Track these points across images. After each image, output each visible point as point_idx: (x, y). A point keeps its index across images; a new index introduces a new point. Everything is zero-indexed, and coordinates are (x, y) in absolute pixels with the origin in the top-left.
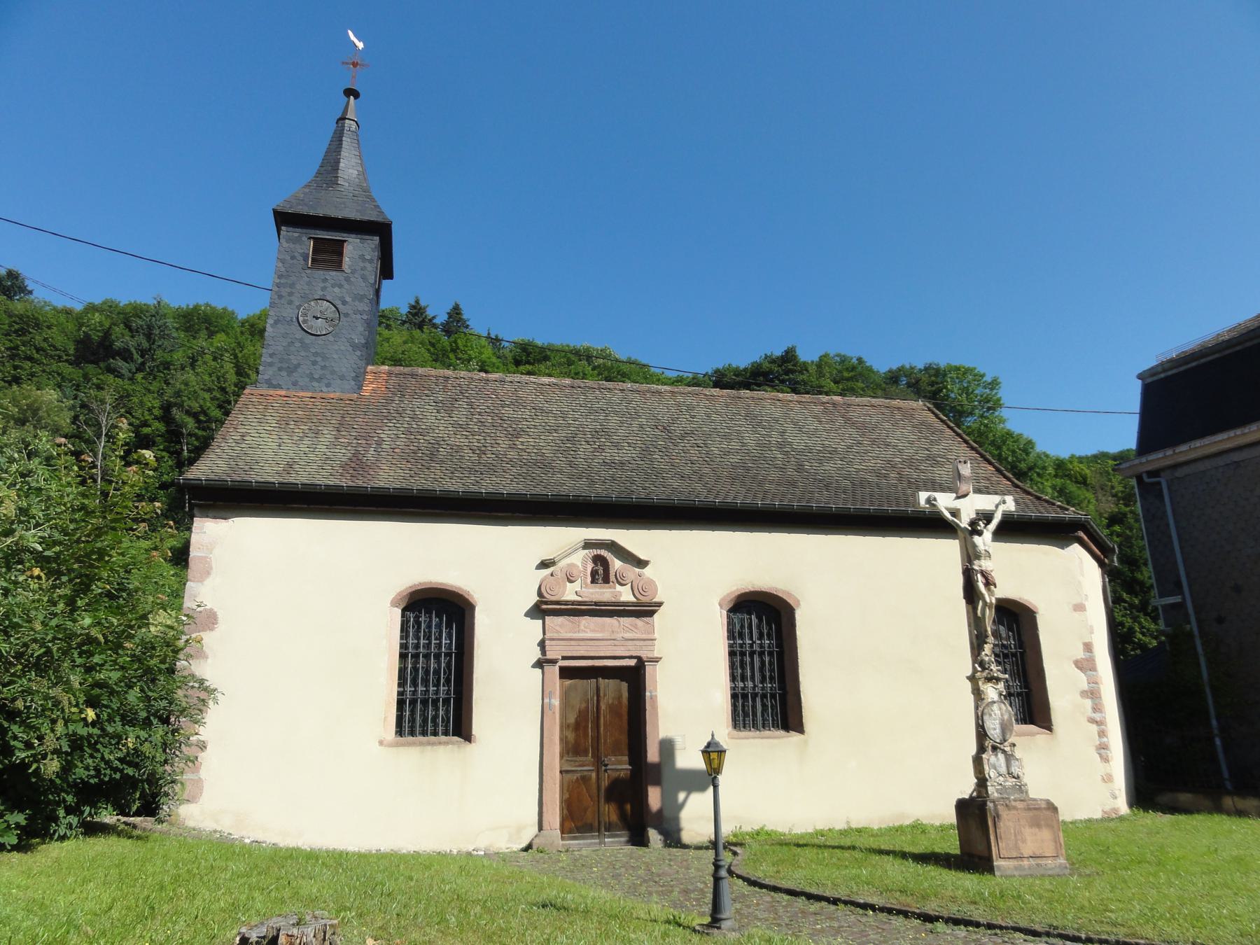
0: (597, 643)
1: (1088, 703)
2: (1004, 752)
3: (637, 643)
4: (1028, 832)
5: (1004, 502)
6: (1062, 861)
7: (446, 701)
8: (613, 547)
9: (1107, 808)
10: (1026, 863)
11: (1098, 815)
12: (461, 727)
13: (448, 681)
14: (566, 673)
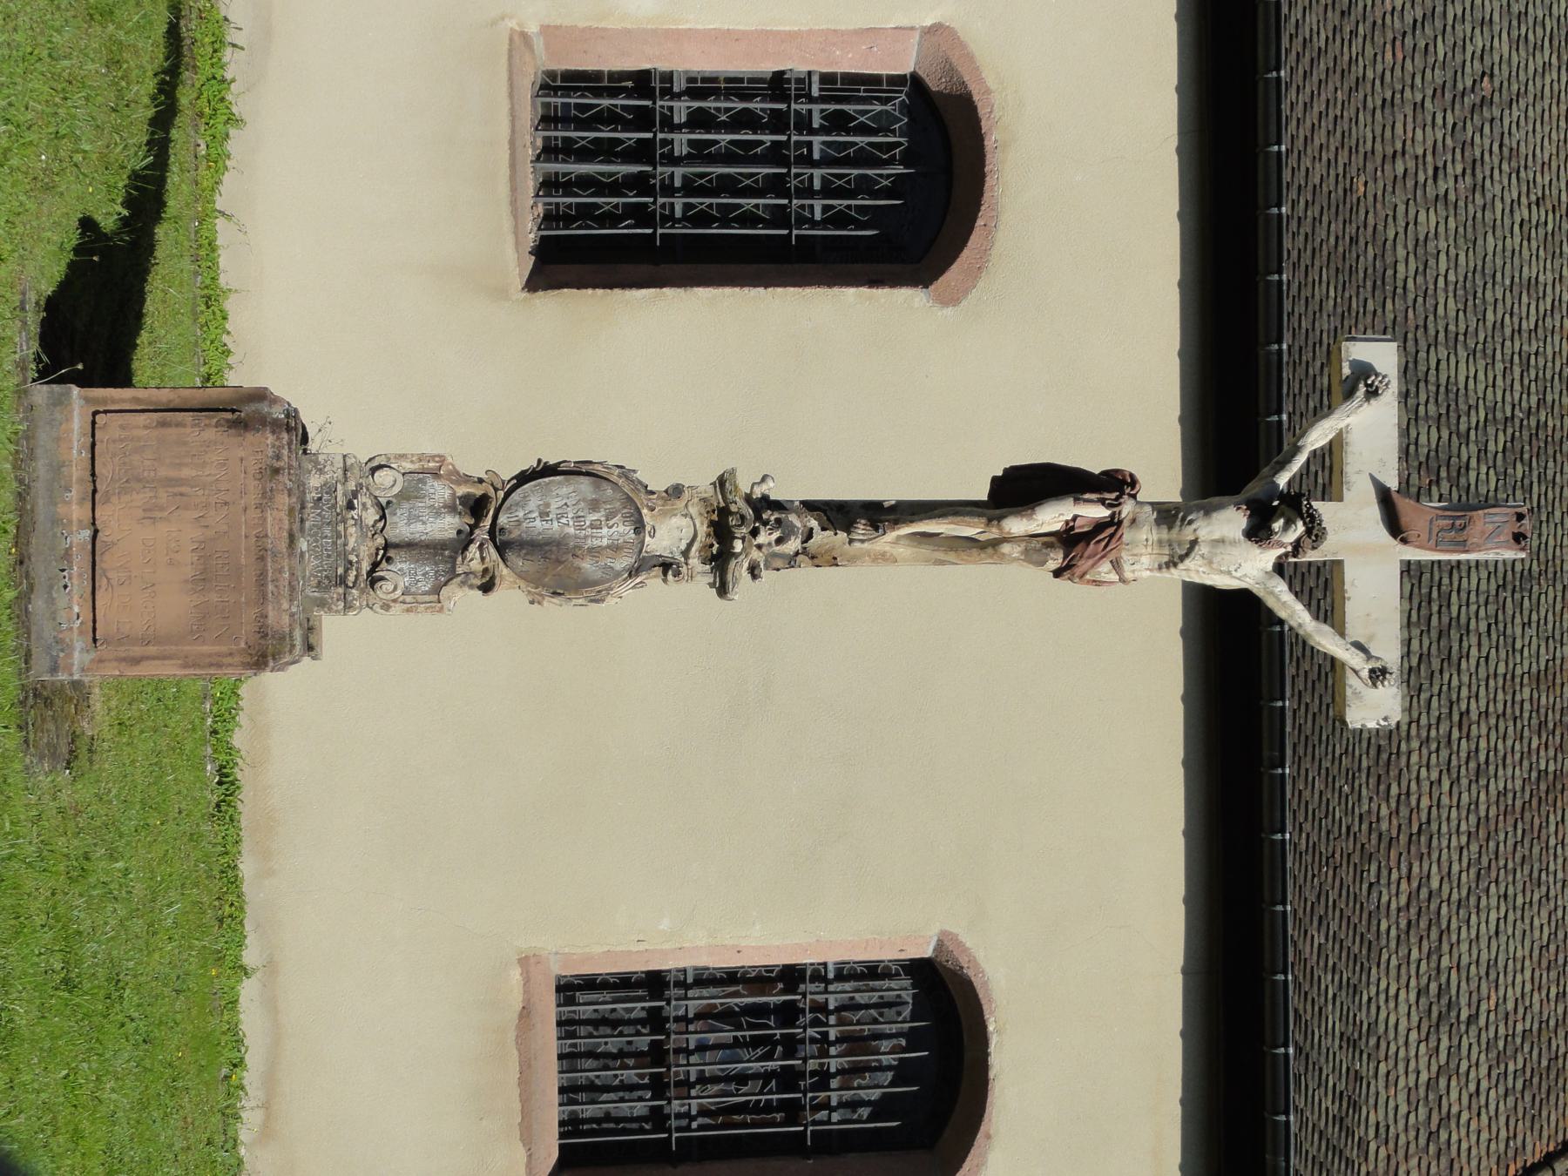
2: (463, 542)
5: (1378, 675)
6: (80, 656)
7: (641, 215)
10: (78, 511)
13: (703, 219)
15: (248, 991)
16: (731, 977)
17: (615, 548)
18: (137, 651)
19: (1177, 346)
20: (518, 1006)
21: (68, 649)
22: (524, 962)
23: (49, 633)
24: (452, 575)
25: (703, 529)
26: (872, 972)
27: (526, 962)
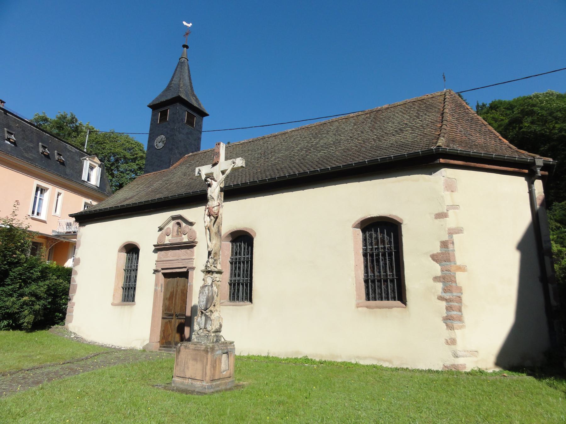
0: (172, 262)
1: (439, 286)
2: (206, 316)
3: (186, 261)
4: (191, 363)
8: (180, 217)
9: (448, 364)
10: (186, 381)
11: (438, 367)
12: (249, 298)
14: (166, 275)
15: (362, 362)
16: (366, 267)
17: (208, 290)
18: (204, 373)
19: (302, 191)
20: (365, 309)
21: (203, 385)
22: (358, 307)
23: (201, 389)
24: (209, 318)
25: (209, 275)
26: (365, 240)
27: (358, 306)
